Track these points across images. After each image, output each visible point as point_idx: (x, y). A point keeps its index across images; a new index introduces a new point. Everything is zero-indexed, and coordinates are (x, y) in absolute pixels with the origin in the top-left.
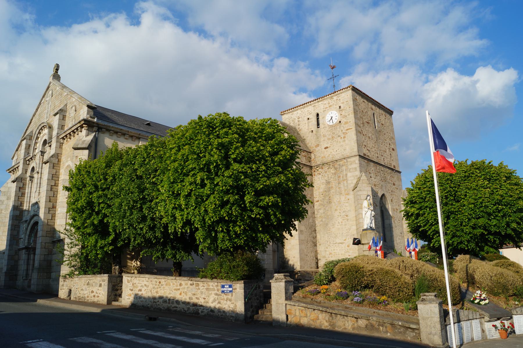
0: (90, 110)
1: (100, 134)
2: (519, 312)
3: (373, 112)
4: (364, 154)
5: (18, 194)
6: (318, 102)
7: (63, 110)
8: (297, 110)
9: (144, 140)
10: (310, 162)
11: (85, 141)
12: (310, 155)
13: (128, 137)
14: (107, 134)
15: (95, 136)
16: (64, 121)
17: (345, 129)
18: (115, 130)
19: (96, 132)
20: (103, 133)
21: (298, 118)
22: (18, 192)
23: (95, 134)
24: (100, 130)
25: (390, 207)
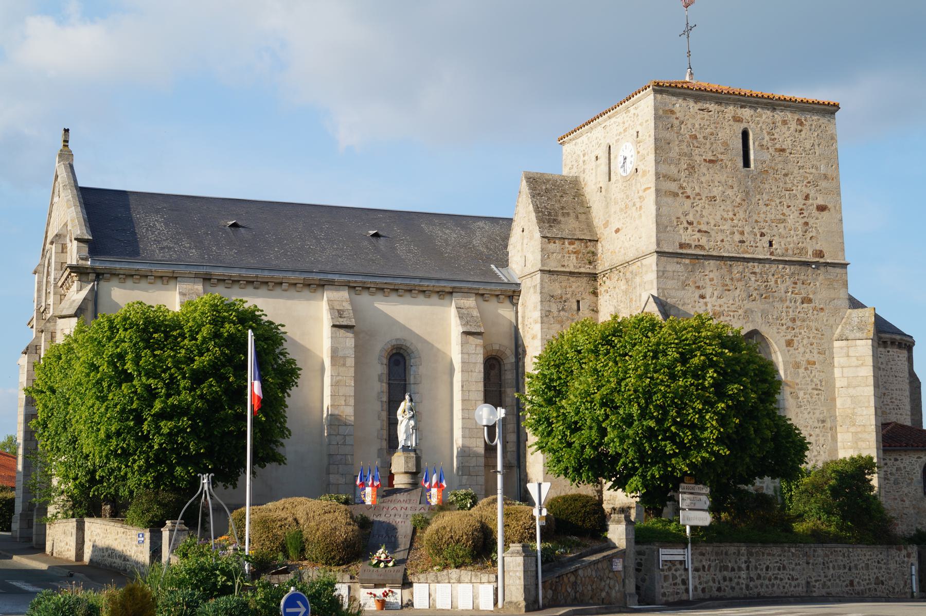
0: (81, 244)
1: (102, 283)
2: (422, 580)
3: (743, 125)
4: (682, 246)
5: (32, 375)
6: (610, 118)
7: (60, 235)
8: (582, 134)
9: (184, 279)
10: (590, 263)
11: (74, 301)
12: (595, 246)
13: (152, 281)
14: (115, 281)
15: (92, 289)
16: (65, 254)
17: (643, 187)
18: (127, 272)
19: (94, 281)
20: (108, 280)
21: (584, 155)
22: (31, 372)
23: (94, 285)
24: (101, 277)
25: (780, 359)
